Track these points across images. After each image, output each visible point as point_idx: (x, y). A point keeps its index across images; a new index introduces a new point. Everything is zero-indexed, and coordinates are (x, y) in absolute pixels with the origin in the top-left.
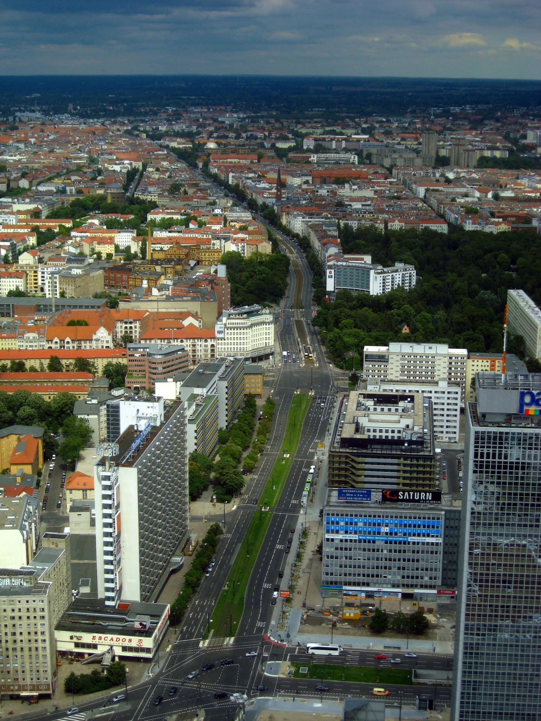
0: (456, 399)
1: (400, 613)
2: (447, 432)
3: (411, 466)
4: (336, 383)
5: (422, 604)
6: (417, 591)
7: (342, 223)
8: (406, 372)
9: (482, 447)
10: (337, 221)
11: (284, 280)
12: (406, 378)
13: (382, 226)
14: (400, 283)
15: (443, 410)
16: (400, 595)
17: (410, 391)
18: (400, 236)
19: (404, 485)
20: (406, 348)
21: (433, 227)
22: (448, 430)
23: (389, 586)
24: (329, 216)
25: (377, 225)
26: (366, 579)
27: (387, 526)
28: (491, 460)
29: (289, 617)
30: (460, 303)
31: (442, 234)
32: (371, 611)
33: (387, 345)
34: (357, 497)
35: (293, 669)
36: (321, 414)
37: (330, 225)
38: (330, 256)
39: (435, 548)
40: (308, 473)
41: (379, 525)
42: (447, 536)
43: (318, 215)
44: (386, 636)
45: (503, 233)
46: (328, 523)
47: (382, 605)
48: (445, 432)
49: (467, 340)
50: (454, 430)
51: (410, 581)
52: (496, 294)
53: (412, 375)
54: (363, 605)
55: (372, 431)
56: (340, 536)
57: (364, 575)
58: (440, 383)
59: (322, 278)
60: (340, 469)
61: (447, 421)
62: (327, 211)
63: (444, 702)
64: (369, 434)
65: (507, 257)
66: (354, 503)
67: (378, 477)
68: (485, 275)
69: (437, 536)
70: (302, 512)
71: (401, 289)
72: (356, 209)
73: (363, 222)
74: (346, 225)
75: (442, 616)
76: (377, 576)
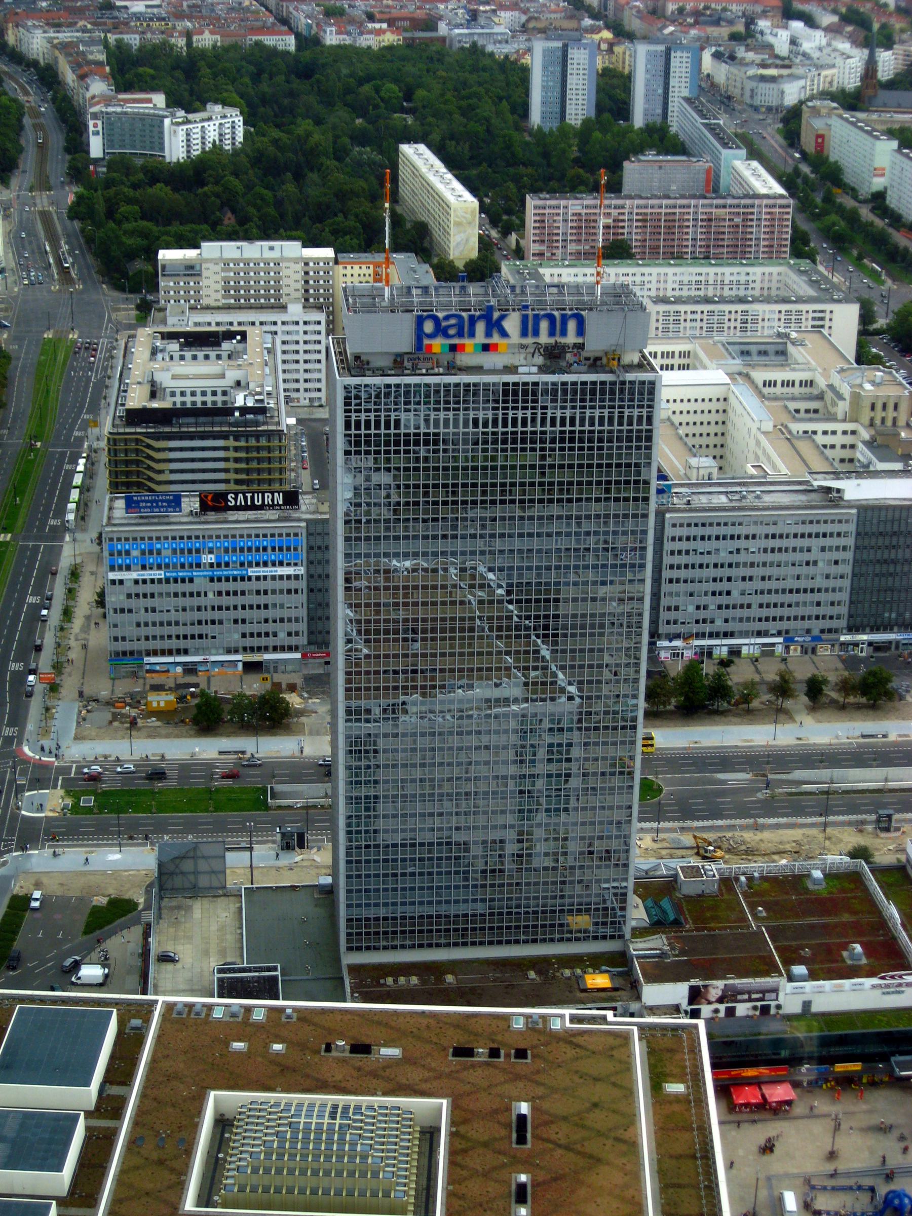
0: (319, 333)
1: (241, 696)
2: (306, 390)
3: (247, 449)
4: (114, 316)
5: (277, 678)
6: (267, 656)
7: (112, 38)
8: (232, 292)
9: (514, 408)
10: (102, 35)
11: (16, 142)
12: (232, 301)
13: (181, 42)
14: (217, 139)
15: (297, 352)
16: (240, 665)
17: (240, 324)
18: (215, 57)
19: (237, 482)
20: (230, 249)
21: (269, 41)
22: (308, 385)
23: (221, 651)
24: (89, 26)
25: (173, 40)
26: (182, 644)
27: (211, 552)
28: (373, 431)
29: (56, 716)
30: (319, 170)
31: (286, 53)
32: (193, 695)
33: (197, 246)
34: (157, 506)
35: (69, 802)
36: (91, 370)
37: (92, 42)
38: (94, 97)
39: (293, 584)
40: (72, 473)
41: (198, 551)
42: (312, 563)
43: (72, 25)
44: (221, 735)
45: (390, 48)
46: (112, 554)
47: (212, 683)
48: (302, 390)
49: (335, 232)
50: (318, 385)
51: (255, 642)
52: (381, 152)
53: (242, 296)
54: (179, 686)
55: (178, 394)
56: (134, 575)
57: (178, 637)
58: (290, 307)
59: (81, 135)
60: (127, 463)
61: (306, 371)
62: (86, 19)
63: (322, 835)
64: (174, 399)
65: (396, 88)
66: (153, 517)
67: (193, 471)
68: (361, 120)
69: (296, 564)
70: (67, 538)
71: (217, 148)
72: (135, 14)
73: (149, 36)
74: (119, 42)
75: (312, 695)
76: (200, 637)
